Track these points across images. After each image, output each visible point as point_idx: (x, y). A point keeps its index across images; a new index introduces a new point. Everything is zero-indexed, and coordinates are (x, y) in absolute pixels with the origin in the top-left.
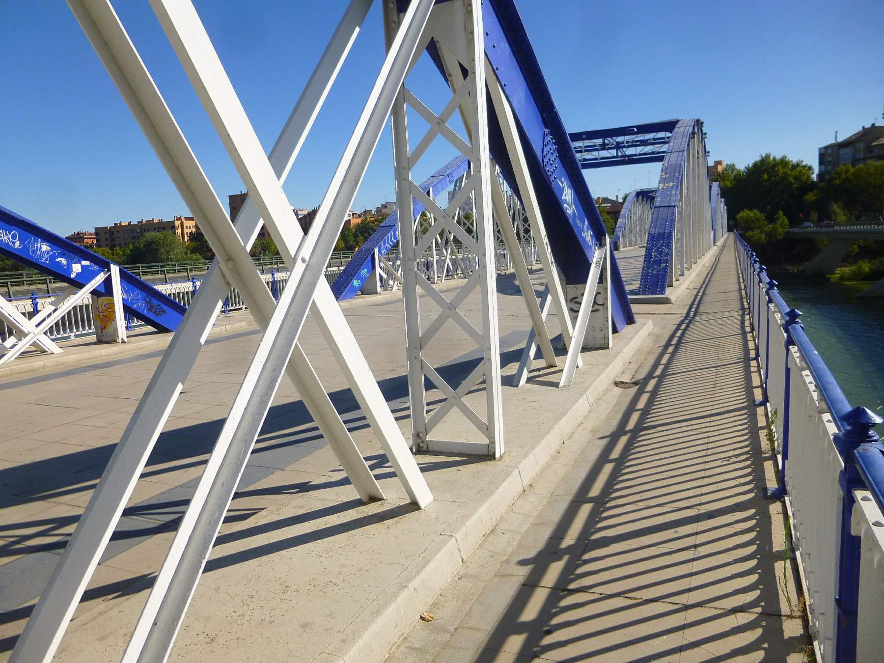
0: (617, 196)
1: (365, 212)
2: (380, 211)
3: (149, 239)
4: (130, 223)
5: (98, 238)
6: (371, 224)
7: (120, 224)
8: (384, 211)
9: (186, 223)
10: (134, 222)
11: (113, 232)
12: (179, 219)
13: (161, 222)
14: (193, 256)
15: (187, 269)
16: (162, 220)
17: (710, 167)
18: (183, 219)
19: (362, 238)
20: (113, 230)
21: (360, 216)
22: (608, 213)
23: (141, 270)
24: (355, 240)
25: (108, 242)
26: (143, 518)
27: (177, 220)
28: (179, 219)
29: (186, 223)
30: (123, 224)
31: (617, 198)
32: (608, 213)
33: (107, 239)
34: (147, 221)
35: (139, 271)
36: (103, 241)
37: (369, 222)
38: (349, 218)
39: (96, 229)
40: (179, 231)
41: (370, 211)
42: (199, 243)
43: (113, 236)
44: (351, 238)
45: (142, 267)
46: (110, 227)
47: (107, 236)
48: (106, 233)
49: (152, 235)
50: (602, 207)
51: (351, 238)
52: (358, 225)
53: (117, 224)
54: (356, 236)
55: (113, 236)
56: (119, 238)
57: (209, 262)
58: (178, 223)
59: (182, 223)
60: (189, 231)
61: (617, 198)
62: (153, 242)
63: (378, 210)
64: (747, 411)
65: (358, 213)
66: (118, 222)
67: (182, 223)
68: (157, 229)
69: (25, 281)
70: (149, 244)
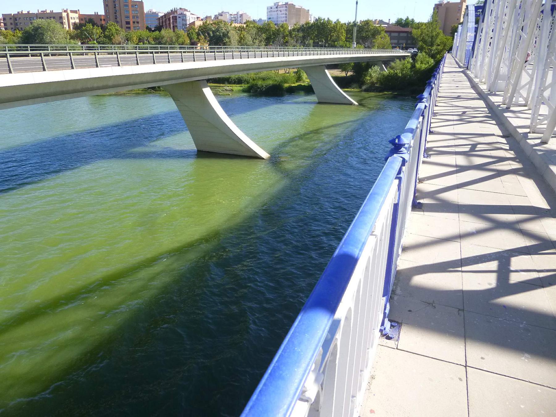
0: (389, 19)
1: (207, 17)
2: (218, 18)
3: (36, 25)
4: (28, 12)
5: (5, 22)
6: (210, 26)
7: (22, 12)
8: (220, 18)
9: (71, 15)
10: (25, 12)
11: (16, 18)
12: (65, 11)
13: (52, 12)
14: (72, 41)
15: (95, 53)
16: (53, 11)
17: (510, 148)
18: (69, 12)
19: (203, 37)
20: (16, 17)
21: (202, 20)
22: (386, 32)
23: (274, 50)
24: (198, 38)
25: (13, 26)
26: (312, 149)
27: (64, 12)
28: (65, 11)
29: (71, 15)
30: (24, 12)
31: (389, 21)
32: (386, 32)
33: (11, 24)
34: (42, 11)
35: (136, 51)
36: (9, 24)
37: (209, 24)
38: (194, 20)
39: (3, 15)
40: (65, 21)
41: (210, 17)
42: (79, 31)
43: (16, 22)
44: (195, 36)
45: (30, 47)
46: (14, 14)
47: (12, 21)
48: (11, 19)
49: (37, 22)
50: (382, 27)
51: (195, 36)
52: (200, 27)
53: (19, 12)
54: (198, 34)
55: (16, 22)
56: (21, 23)
57: (252, 48)
58: (64, 15)
59: (68, 15)
60: (72, 21)
61: (389, 21)
62: (40, 28)
63: (216, 17)
64: (534, 148)
65: (202, 17)
66: (20, 11)
67: (68, 15)
68: (49, 18)
69: (113, 52)
70: (36, 29)
